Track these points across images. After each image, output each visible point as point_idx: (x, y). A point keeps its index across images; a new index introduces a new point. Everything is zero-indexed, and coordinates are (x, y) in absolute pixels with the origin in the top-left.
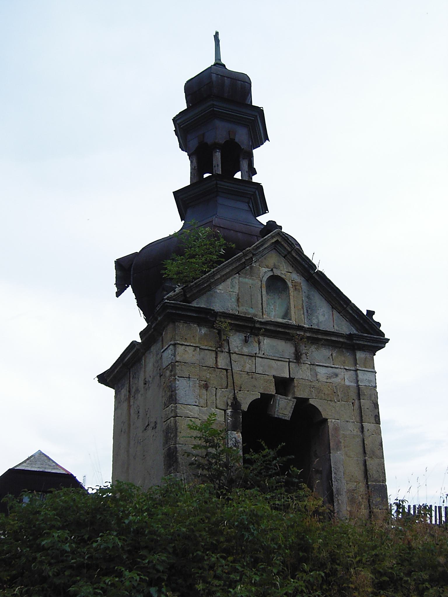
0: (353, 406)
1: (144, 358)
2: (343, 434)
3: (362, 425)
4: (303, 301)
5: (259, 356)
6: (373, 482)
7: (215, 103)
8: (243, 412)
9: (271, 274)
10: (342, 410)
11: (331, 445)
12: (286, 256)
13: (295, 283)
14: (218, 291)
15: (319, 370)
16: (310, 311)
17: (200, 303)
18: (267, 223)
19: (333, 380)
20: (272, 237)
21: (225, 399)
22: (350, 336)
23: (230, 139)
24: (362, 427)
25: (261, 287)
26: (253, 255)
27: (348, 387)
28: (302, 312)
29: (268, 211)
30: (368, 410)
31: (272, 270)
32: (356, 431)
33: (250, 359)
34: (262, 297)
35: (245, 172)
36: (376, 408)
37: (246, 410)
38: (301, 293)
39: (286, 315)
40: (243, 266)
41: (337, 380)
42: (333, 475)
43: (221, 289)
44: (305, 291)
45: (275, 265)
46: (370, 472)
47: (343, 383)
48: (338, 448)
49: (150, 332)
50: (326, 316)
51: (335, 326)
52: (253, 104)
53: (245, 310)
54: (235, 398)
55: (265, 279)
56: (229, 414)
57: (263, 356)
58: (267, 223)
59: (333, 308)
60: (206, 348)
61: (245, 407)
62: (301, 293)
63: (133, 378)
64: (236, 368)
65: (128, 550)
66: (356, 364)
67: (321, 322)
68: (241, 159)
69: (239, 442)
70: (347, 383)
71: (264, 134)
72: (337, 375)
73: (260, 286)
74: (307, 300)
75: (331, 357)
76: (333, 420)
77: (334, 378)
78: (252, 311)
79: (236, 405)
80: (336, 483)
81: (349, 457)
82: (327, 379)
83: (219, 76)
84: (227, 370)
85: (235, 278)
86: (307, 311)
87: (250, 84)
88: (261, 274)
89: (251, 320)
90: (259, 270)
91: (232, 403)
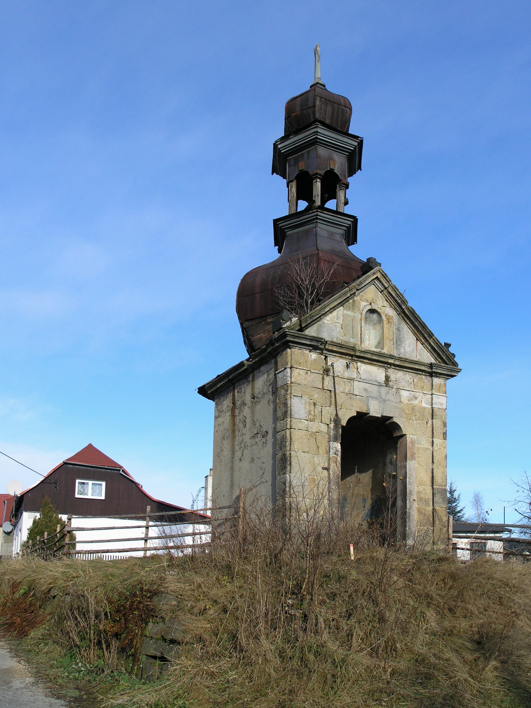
0: (427, 424)
1: (251, 376)
2: (418, 447)
3: (433, 440)
4: (393, 333)
5: (357, 379)
6: (437, 486)
7: (319, 130)
8: (343, 427)
9: (369, 307)
10: (418, 427)
11: (408, 456)
12: (382, 291)
13: (389, 316)
14: (326, 322)
15: (403, 393)
16: (398, 341)
17: (311, 332)
18: (367, 259)
19: (413, 402)
20: (374, 274)
21: (329, 416)
22: (431, 366)
23: (330, 169)
24: (433, 442)
25: (361, 319)
26: (357, 290)
27: (424, 408)
28: (392, 343)
29: (356, 242)
30: (438, 428)
31: (371, 304)
32: (428, 446)
33: (349, 382)
34: (361, 328)
35: (342, 203)
36: (444, 427)
37: (345, 425)
38: (392, 326)
39: (380, 344)
40: (347, 300)
41: (416, 402)
42: (408, 480)
43: (327, 320)
44: (396, 324)
45: (373, 299)
46: (436, 479)
47: (420, 405)
48: (413, 458)
49: (264, 355)
50: (412, 347)
51: (418, 356)
52: (349, 132)
53: (347, 340)
54: (337, 415)
55: (364, 312)
56: (332, 428)
57: (360, 380)
58: (367, 259)
59: (417, 339)
60: (315, 371)
61: (344, 423)
62: (392, 326)
63: (238, 392)
64: (339, 389)
65: (25, 546)
66: (432, 389)
67: (407, 352)
68: (338, 188)
69: (339, 451)
70: (424, 405)
71: (358, 164)
72: (416, 398)
73: (360, 318)
74: (397, 332)
75: (412, 383)
76: (411, 436)
77: (413, 400)
78: (352, 340)
79: (337, 420)
80: (410, 486)
81: (421, 466)
82: (409, 401)
83: (323, 99)
84: (330, 391)
85: (340, 310)
86: (397, 342)
87: (351, 109)
88: (361, 308)
89: (353, 349)
90: (360, 304)
91: (334, 419)
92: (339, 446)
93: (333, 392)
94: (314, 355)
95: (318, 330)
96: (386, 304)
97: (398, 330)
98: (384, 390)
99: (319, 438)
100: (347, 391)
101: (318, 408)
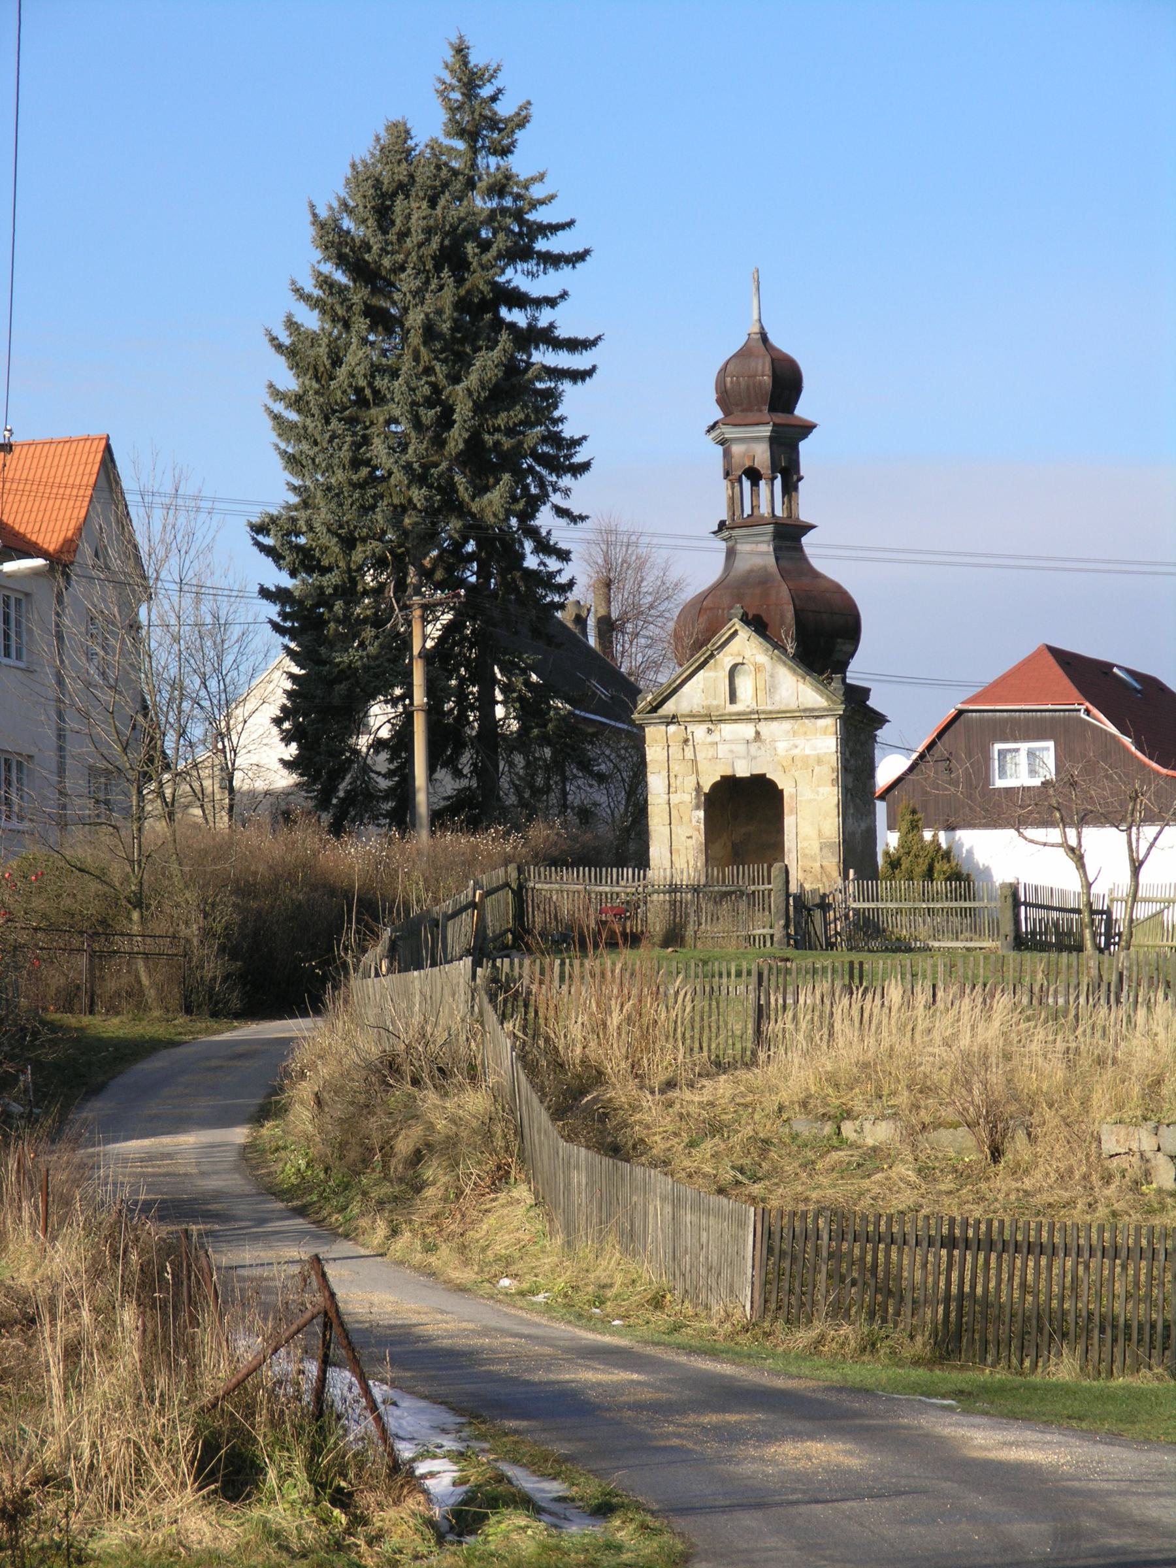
8: (705, 794)
61: (706, 789)
78: (715, 703)
92: (701, 814)
93: (694, 761)
94: (672, 728)
95: (677, 703)
96: (755, 651)
97: (772, 676)
98: (753, 748)
99: (682, 808)
100: (710, 756)
101: (680, 779)
